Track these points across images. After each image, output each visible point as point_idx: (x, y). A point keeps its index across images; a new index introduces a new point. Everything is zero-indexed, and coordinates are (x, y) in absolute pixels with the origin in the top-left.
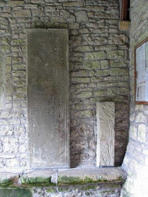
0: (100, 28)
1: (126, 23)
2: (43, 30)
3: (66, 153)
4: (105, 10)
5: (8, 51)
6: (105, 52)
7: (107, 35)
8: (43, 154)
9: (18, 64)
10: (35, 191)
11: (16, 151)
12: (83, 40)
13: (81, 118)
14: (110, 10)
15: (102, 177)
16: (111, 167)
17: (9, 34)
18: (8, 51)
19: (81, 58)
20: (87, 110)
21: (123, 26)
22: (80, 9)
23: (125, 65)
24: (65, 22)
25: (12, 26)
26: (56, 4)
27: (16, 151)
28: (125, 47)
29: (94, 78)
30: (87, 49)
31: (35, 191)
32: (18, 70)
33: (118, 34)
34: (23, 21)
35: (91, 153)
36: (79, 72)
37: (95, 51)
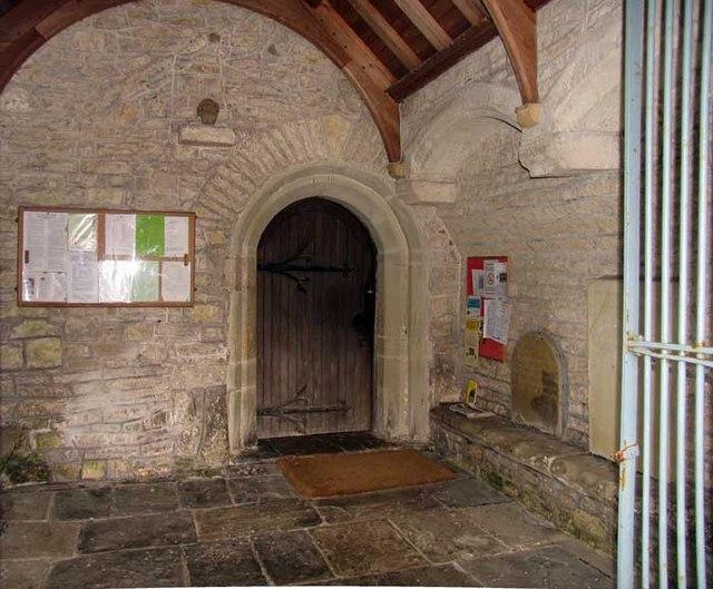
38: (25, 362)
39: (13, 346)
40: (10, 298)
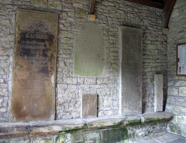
0: (155, 31)
1: (167, 29)
2: (130, 28)
3: (140, 105)
4: (157, 20)
5: (108, 38)
6: (157, 45)
7: (157, 35)
8: (129, 106)
9: (113, 47)
10: (129, 129)
11: (111, 105)
12: (147, 37)
13: (146, 84)
14: (159, 20)
15: (164, 117)
16: (161, 112)
17: (107, 27)
18: (108, 38)
19: (146, 47)
20: (148, 79)
21: (165, 31)
22: (145, 18)
23: (165, 54)
24: (138, 24)
25: (109, 22)
26: (134, 12)
27: (111, 105)
28: (165, 43)
29: (152, 60)
30: (149, 42)
31: (129, 129)
32: (113, 52)
33: (163, 35)
34: (116, 20)
35: (150, 105)
36: (145, 56)
37: (152, 44)
38: (178, 94)
39: (176, 88)
40: (175, 73)
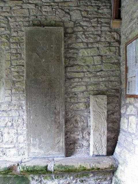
0: (93, 27)
1: (118, 21)
2: (40, 28)
4: (98, 9)
5: (7, 48)
6: (98, 48)
7: (99, 33)
8: (40, 144)
9: (17, 60)
10: (33, 178)
11: (15, 141)
13: (76, 110)
14: (102, 9)
15: (95, 166)
16: (103, 156)
17: (8, 32)
18: (7, 48)
19: (76, 54)
20: (81, 103)
21: (115, 24)
22: (75, 8)
23: (116, 61)
24: (60, 21)
25: (11, 24)
26: (52, 4)
27: (15, 141)
28: (116, 44)
29: (88, 73)
30: (81, 45)
31: (33, 178)
32: (17, 65)
33: (110, 32)
34: (22, 19)
35: (85, 143)
36: (74, 68)
37: (89, 48)
